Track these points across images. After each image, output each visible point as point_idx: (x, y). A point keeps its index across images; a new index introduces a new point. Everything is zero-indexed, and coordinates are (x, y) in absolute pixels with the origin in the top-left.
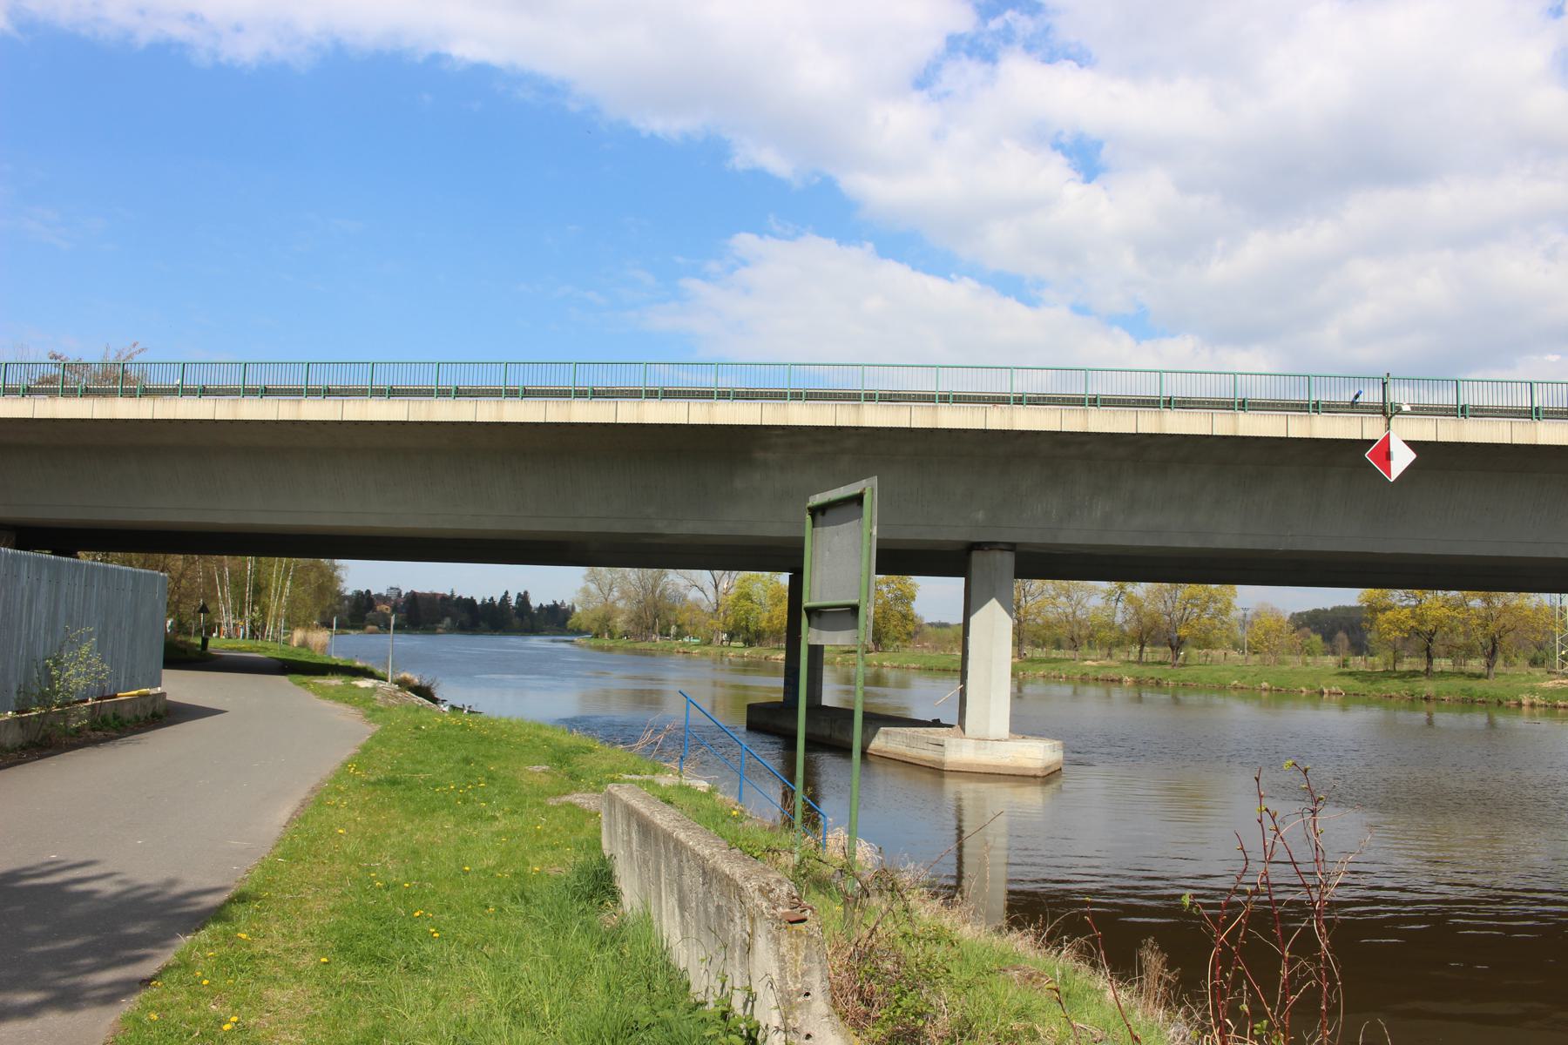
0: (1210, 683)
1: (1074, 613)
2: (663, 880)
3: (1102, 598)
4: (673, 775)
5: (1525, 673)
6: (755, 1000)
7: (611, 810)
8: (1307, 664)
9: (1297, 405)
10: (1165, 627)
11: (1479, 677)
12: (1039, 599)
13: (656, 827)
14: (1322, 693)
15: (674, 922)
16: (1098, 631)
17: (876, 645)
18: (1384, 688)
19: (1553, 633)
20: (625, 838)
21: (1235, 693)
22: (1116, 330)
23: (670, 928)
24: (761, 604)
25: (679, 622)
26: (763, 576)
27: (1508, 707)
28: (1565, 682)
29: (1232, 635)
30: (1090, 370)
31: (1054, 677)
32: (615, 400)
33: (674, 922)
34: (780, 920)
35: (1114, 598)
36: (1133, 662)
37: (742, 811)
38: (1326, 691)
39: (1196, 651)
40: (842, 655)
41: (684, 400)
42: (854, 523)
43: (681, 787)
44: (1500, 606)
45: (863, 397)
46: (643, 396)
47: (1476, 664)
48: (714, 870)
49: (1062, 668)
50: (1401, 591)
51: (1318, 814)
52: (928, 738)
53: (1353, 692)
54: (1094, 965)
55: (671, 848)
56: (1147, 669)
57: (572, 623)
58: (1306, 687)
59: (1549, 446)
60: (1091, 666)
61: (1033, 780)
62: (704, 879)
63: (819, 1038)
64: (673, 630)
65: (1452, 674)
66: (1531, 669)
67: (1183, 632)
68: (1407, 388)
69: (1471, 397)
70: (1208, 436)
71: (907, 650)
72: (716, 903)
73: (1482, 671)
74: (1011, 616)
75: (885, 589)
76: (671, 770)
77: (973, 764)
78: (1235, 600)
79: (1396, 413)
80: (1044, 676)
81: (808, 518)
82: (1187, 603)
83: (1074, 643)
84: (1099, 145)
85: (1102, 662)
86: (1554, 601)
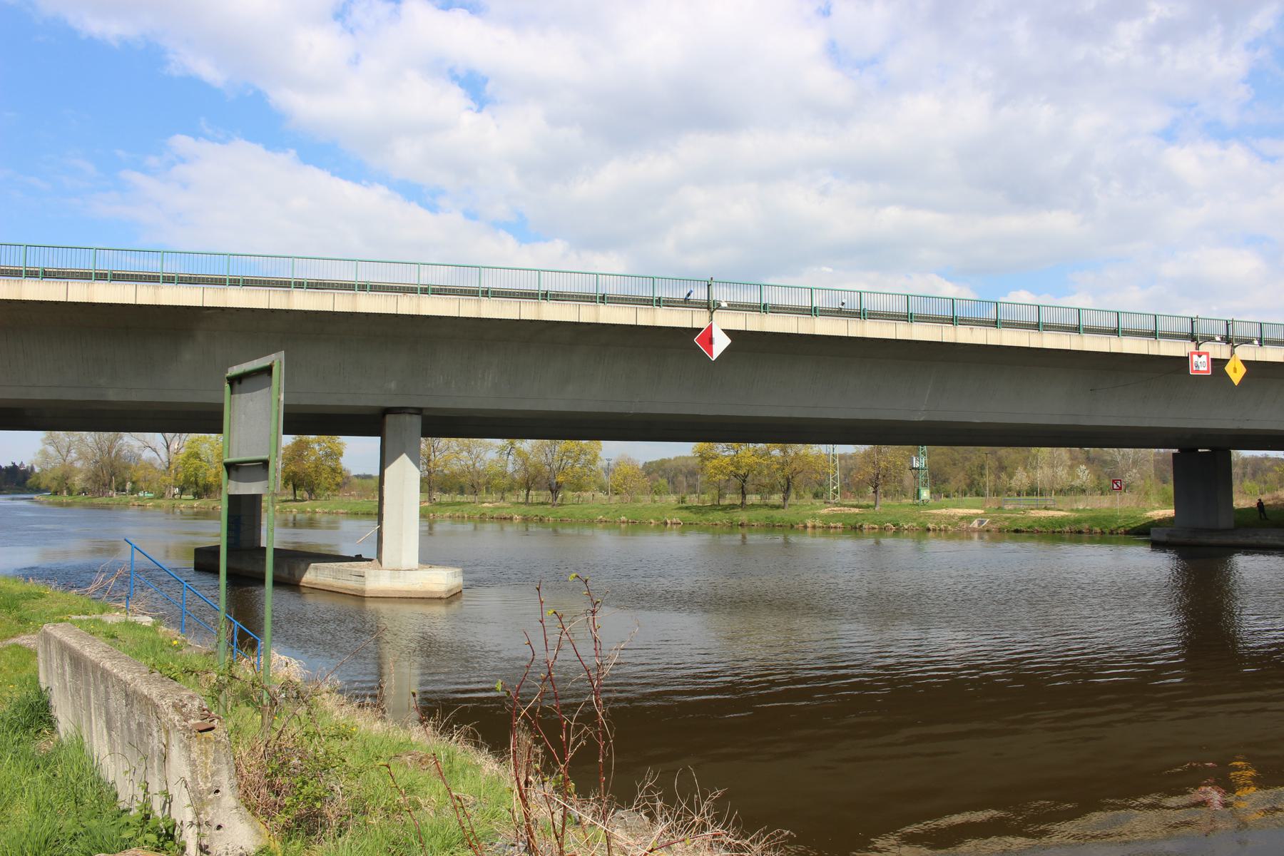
0: (581, 518)
1: (474, 465)
2: (92, 706)
3: (497, 453)
4: (121, 613)
5: (810, 504)
6: (172, 801)
7: (46, 648)
8: (655, 502)
9: (644, 300)
10: (546, 475)
11: (778, 507)
12: (445, 454)
13: (86, 658)
14: (666, 523)
15: (103, 742)
16: (493, 479)
17: (310, 495)
18: (711, 518)
19: (828, 474)
20: (60, 671)
21: (601, 525)
22: (502, 234)
23: (99, 745)
24: (208, 462)
25: (134, 479)
26: (210, 437)
27: (798, 529)
28: (835, 509)
29: (598, 481)
30: (482, 267)
31: (459, 517)
32: (67, 280)
33: (103, 742)
34: (191, 730)
35: (506, 452)
36: (522, 503)
37: (183, 641)
38: (669, 521)
39: (570, 493)
40: (282, 504)
41: (133, 283)
42: (265, 390)
43: (127, 623)
44: (792, 455)
45: (93, 276)
46: (93, 278)
47: (776, 498)
48: (135, 692)
49: (464, 509)
50: (723, 444)
51: (596, 614)
52: (351, 571)
53: (688, 523)
54: (477, 745)
55: (99, 676)
56: (532, 508)
57: (31, 482)
58: (654, 519)
59: (823, 336)
60: (488, 508)
61: (439, 601)
62: (127, 701)
63: (229, 828)
64: (129, 486)
65: (759, 506)
66: (813, 501)
67: (560, 479)
68: (725, 288)
69: (772, 298)
70: (455, 317)
71: (337, 498)
72: (137, 721)
73: (780, 503)
74: (418, 467)
75: (317, 448)
76: (118, 609)
77: (389, 590)
78: (601, 452)
79: (717, 308)
80: (450, 517)
81: (227, 386)
82: (563, 455)
83: (475, 489)
84: (486, 81)
85: (496, 504)
86: (829, 450)
